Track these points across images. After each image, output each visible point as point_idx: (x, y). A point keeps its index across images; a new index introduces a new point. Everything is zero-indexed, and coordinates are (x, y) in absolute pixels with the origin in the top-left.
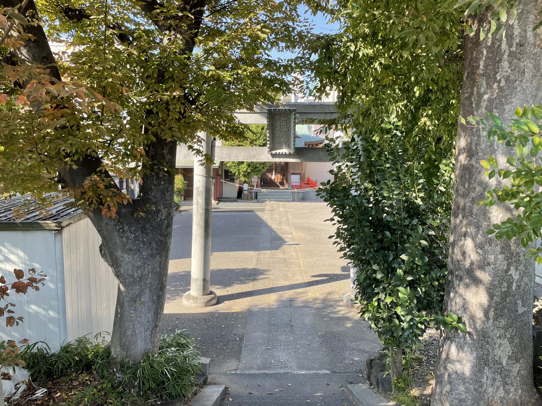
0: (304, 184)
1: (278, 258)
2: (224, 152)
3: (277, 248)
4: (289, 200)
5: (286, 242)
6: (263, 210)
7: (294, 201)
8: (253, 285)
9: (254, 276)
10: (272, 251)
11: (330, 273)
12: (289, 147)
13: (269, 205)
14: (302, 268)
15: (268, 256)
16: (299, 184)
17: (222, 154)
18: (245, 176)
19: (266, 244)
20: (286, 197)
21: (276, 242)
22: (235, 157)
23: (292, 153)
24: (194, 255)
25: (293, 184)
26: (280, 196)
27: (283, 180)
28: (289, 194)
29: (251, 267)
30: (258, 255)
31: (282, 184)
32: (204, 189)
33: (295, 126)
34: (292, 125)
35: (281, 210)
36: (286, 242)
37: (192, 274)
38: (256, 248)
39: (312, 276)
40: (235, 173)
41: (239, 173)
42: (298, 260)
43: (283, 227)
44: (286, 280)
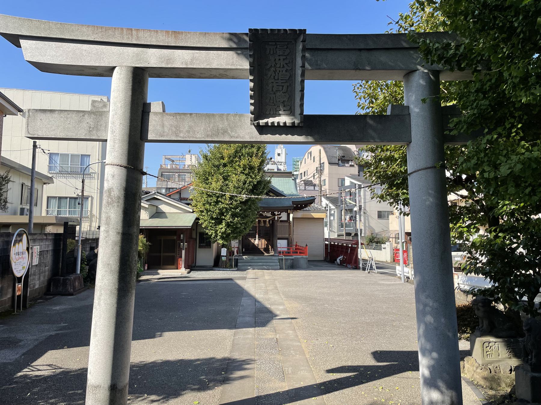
1: (266, 339)
2: (166, 123)
3: (263, 324)
4: (276, 267)
5: (276, 316)
6: (244, 278)
7: (281, 268)
8: (223, 392)
9: (226, 373)
10: (257, 329)
11: (360, 364)
12: (291, 112)
13: (251, 273)
14: (308, 356)
15: (250, 336)
16: (286, 249)
17: (163, 126)
18: (222, 238)
19: (248, 319)
20: (271, 264)
21: (262, 316)
22: (188, 132)
23: (297, 122)
24: (95, 332)
25: (279, 249)
27: (267, 245)
28: (276, 261)
29: (220, 355)
30: (235, 335)
31: (267, 250)
32: (123, 192)
33: (302, 82)
34: (299, 79)
35: (267, 277)
36: (276, 316)
37: (89, 376)
38: (232, 324)
39: (329, 371)
40: (212, 235)
41: (216, 236)
42: (299, 342)
43: (271, 296)
44: (283, 380)
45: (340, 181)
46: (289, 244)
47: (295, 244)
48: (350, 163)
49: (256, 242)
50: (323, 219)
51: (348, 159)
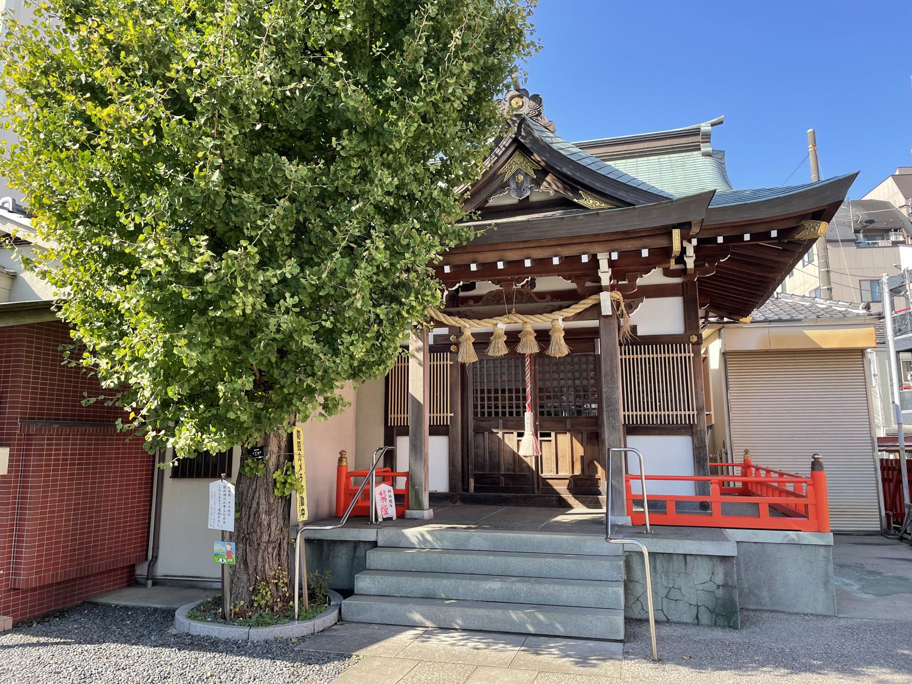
0: (726, 491)
4: (598, 624)
16: (686, 490)
25: (636, 488)
26: (521, 588)
27: (588, 464)
28: (604, 569)
31: (584, 488)
45: (866, 286)
46: (708, 459)
47: (738, 459)
48: (893, 238)
49: (525, 445)
50: (862, 352)
51: (883, 225)
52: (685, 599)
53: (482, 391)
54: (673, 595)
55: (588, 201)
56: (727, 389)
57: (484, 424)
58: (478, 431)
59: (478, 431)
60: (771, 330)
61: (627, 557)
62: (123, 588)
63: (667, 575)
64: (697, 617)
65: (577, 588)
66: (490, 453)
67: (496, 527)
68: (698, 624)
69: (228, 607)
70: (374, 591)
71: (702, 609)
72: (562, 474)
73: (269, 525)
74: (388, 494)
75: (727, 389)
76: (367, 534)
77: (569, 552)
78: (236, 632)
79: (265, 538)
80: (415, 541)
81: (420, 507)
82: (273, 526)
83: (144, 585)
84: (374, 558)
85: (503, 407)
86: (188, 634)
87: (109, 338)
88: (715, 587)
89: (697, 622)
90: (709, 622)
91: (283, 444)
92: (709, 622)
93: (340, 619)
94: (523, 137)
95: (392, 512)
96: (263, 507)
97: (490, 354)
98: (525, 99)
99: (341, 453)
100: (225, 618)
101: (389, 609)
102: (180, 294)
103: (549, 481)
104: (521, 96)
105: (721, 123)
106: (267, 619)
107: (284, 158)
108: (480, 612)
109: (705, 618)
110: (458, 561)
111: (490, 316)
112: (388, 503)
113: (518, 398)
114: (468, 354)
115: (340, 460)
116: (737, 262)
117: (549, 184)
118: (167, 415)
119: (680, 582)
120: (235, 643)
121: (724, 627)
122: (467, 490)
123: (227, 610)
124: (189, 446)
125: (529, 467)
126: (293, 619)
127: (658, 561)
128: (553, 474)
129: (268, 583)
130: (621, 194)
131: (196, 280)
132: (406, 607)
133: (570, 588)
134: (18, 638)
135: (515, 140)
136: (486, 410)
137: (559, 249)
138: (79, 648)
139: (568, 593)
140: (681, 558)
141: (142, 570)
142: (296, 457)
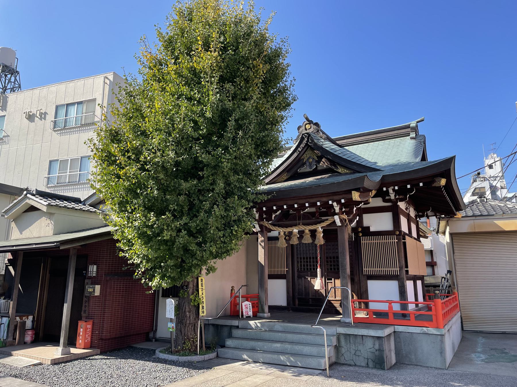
26: (288, 346)
52: (363, 355)
53: (301, 258)
54: (357, 353)
55: (340, 170)
56: (454, 253)
57: (302, 274)
58: (299, 277)
59: (299, 277)
60: (475, 221)
61: (338, 336)
62: (144, 342)
63: (355, 345)
64: (368, 364)
65: (310, 347)
66: (305, 288)
67: (290, 322)
68: (368, 367)
69: (173, 348)
70: (232, 346)
71: (370, 360)
72: (337, 298)
73: (190, 317)
74: (248, 306)
75: (454, 253)
76: (235, 323)
77: (322, 334)
78: (174, 358)
79: (188, 322)
80: (253, 326)
81: (263, 312)
82: (191, 318)
83: (152, 341)
84: (236, 333)
85: (310, 266)
86: (158, 358)
87: (129, 246)
88: (375, 351)
89: (367, 366)
90: (372, 366)
91: (195, 285)
92: (372, 366)
93: (217, 356)
94: (310, 143)
95: (251, 314)
96: (187, 309)
97: (303, 242)
98: (312, 125)
99: (232, 287)
100: (172, 352)
101: (236, 353)
102: (146, 232)
103: (332, 302)
104: (310, 124)
105: (423, 120)
106: (187, 354)
107: (182, 181)
108: (269, 356)
109: (371, 364)
110: (268, 335)
111: (291, 226)
112: (249, 310)
113: (313, 262)
114: (295, 241)
115: (232, 290)
116: (430, 190)
117: (324, 163)
118: (149, 274)
119: (360, 347)
120: (173, 361)
121: (379, 369)
122: (295, 305)
123: (173, 350)
124: (157, 285)
125: (323, 295)
126: (197, 354)
127: (351, 338)
128: (333, 299)
129: (189, 340)
130: (355, 167)
131: (152, 227)
132: (242, 352)
133: (307, 347)
134: (100, 357)
135: (307, 144)
136: (312, 267)
137: (308, 199)
138: (119, 360)
139: (307, 350)
140: (361, 337)
141: (151, 335)
142: (200, 290)
